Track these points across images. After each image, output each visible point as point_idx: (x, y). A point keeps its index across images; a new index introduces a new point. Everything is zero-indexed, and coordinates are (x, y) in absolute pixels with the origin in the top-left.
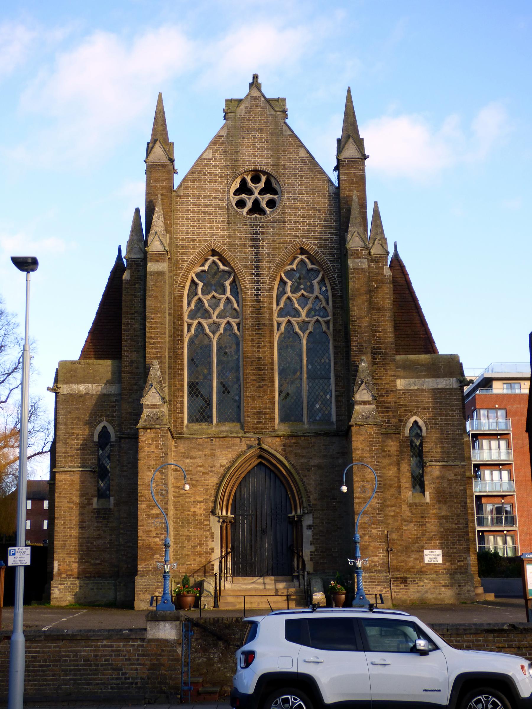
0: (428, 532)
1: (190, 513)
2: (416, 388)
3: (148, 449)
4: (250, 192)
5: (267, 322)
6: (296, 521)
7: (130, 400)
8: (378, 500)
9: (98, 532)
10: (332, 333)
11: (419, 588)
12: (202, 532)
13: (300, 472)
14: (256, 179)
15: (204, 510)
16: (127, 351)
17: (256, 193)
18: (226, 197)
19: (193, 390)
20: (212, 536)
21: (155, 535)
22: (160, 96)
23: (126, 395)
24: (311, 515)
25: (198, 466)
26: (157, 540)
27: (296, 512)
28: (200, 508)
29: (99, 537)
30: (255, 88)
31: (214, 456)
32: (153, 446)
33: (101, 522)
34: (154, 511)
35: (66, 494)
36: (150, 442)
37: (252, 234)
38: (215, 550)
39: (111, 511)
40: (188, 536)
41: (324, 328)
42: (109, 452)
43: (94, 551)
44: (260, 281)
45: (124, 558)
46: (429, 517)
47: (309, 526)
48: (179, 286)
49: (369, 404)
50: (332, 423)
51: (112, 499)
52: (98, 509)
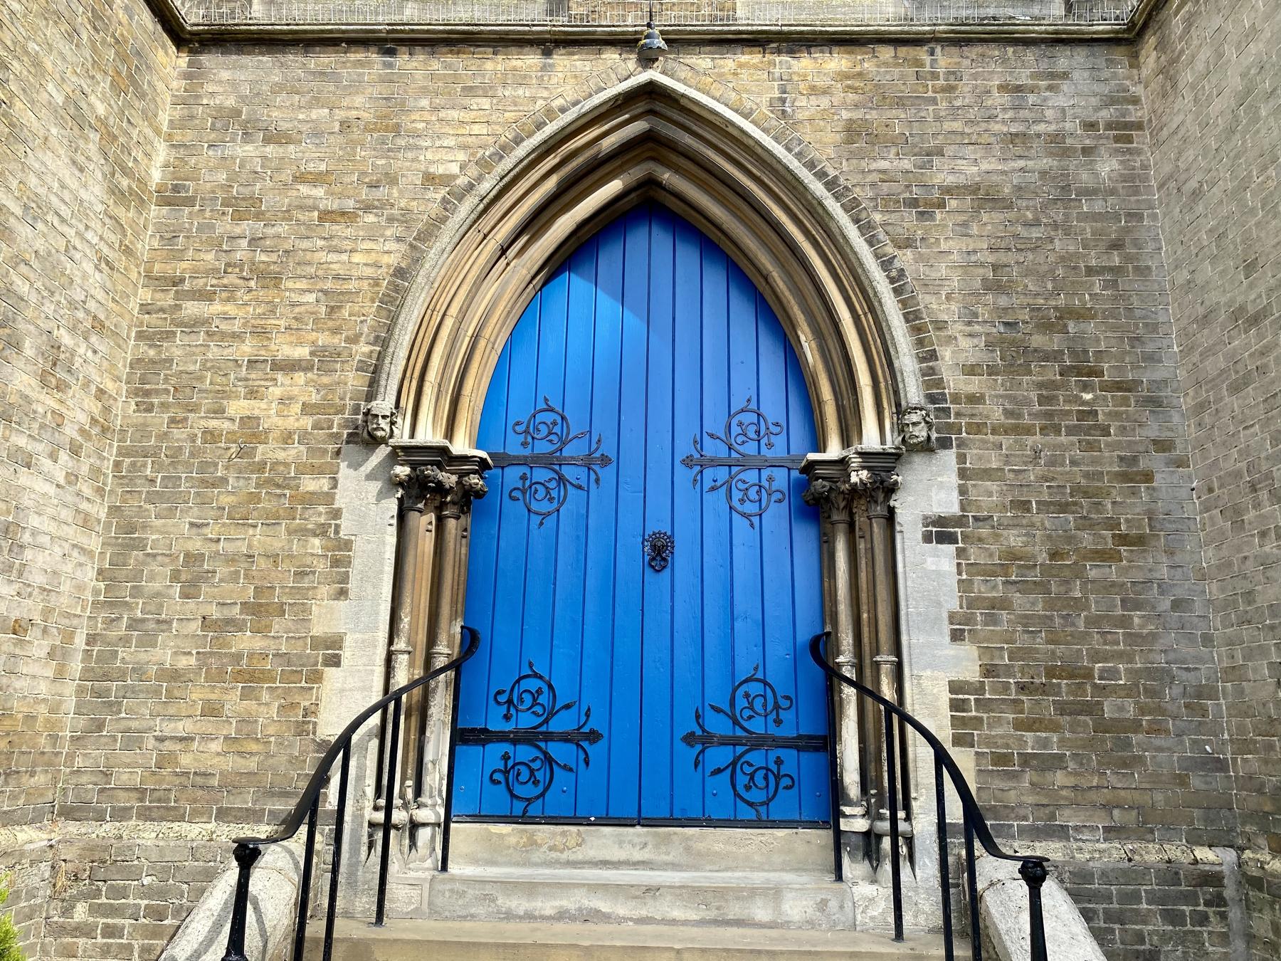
1: (227, 425)
6: (856, 492)
12: (278, 540)
13: (877, 217)
15: (307, 409)
20: (336, 563)
24: (948, 457)
25: (300, 178)
28: (284, 401)
31: (397, 129)
38: (346, 655)
40: (192, 558)
47: (940, 521)
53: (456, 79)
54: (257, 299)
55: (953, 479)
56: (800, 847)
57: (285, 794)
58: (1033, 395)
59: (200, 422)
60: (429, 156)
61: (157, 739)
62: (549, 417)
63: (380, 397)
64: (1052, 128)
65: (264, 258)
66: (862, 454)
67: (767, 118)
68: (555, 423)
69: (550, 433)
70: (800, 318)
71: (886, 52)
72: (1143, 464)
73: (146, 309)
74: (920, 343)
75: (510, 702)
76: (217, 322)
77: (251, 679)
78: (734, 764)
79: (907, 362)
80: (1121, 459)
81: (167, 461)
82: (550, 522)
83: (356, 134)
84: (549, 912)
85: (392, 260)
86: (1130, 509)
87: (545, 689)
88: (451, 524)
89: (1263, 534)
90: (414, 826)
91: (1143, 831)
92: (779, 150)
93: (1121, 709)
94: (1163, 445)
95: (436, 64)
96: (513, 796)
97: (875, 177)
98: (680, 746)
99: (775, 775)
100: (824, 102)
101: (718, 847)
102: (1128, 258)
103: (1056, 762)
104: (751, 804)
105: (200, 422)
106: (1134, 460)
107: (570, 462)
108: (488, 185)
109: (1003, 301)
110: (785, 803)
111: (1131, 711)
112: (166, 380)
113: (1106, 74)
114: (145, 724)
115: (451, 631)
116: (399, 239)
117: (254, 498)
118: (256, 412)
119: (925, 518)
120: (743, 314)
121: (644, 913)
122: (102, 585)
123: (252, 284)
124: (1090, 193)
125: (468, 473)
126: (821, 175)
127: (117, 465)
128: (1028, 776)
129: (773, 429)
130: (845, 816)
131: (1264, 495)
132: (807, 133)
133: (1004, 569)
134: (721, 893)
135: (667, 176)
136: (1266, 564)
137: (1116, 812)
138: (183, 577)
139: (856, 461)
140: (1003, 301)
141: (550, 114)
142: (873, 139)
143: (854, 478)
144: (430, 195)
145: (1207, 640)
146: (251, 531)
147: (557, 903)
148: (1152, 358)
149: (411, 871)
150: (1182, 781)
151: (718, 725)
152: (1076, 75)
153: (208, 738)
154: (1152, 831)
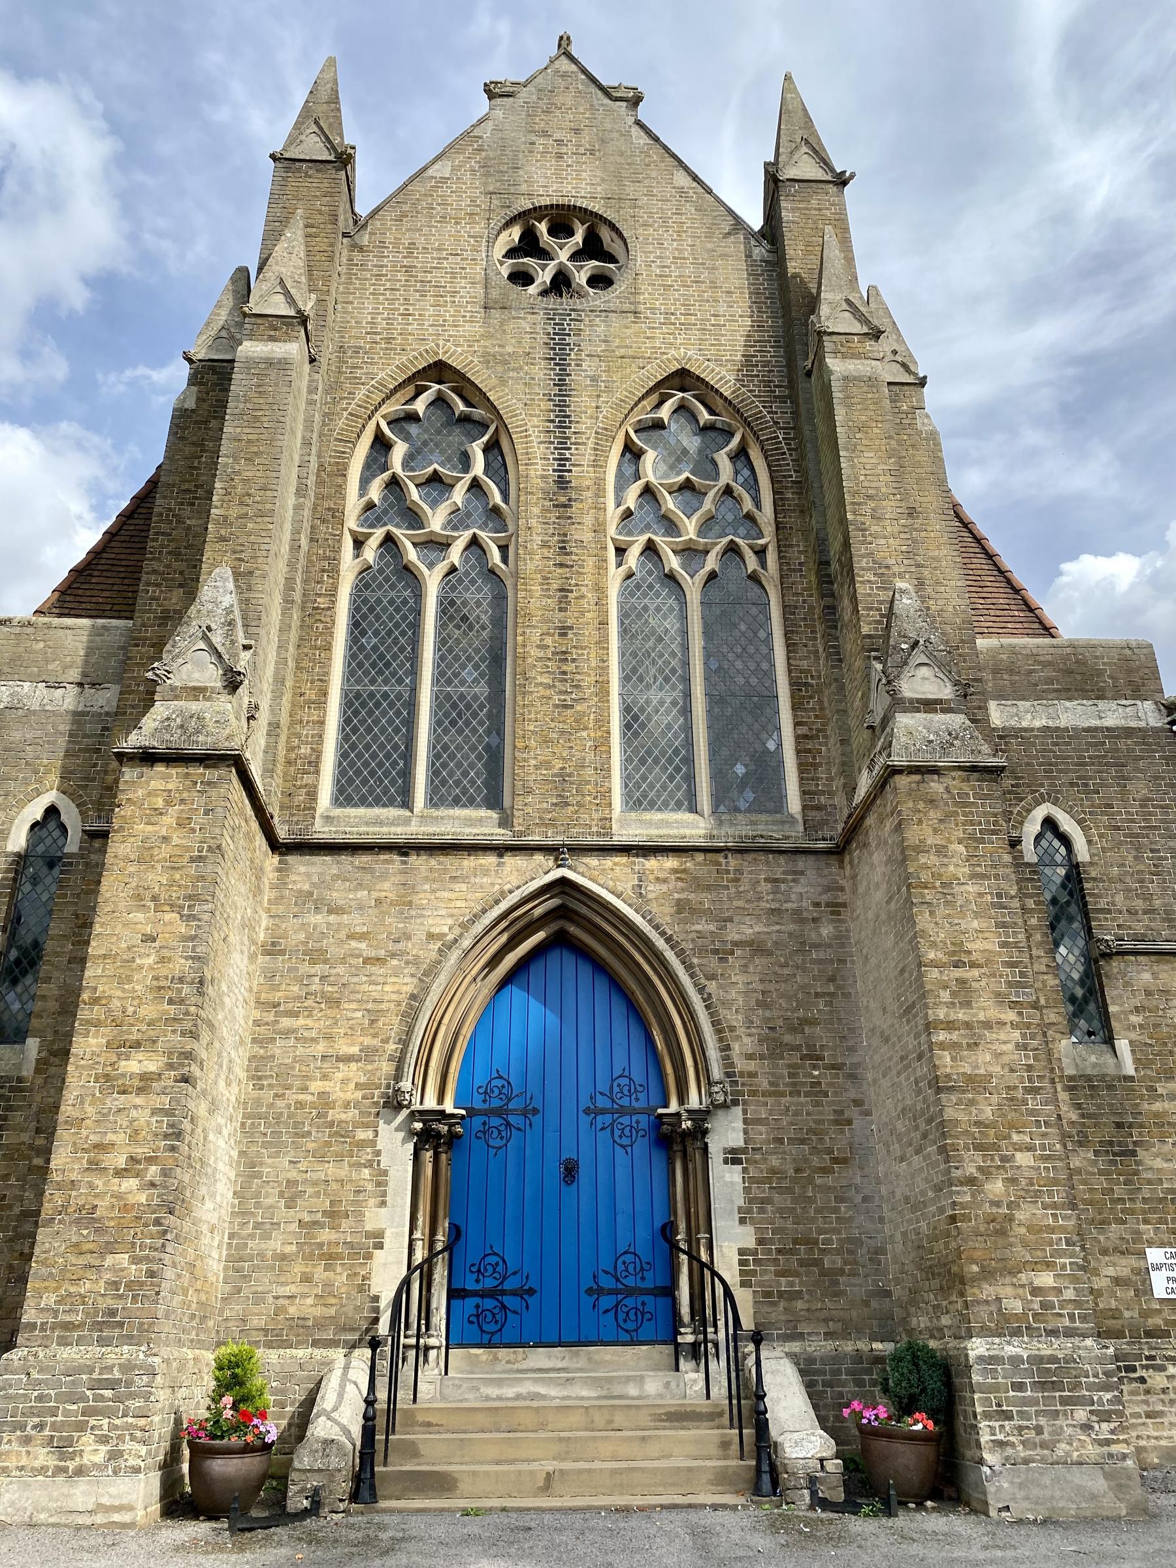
0: (1149, 1182)
1: (309, 1098)
2: (1037, 724)
4: (544, 254)
5: (587, 536)
6: (685, 1134)
8: (1023, 1035)
10: (777, 576)
11: (1152, 1399)
12: (343, 1171)
13: (695, 961)
14: (561, 229)
16: (158, 585)
17: (563, 256)
18: (484, 255)
19: (356, 713)
20: (379, 1184)
21: (121, 1161)
22: (788, 78)
23: (133, 707)
24: (738, 1111)
25: (350, 937)
26: (131, 1183)
27: (682, 1100)
31: (410, 903)
32: (169, 820)
34: (135, 1065)
36: (160, 803)
37: (549, 334)
38: (387, 1241)
39: (21, 1090)
40: (291, 1183)
41: (752, 563)
44: (569, 438)
46: (1141, 1126)
47: (733, 1151)
48: (336, 440)
49: (943, 711)
50: (792, 820)
54: (326, 1016)
55: (740, 1125)
56: (656, 1356)
57: (353, 1330)
58: (785, 1072)
59: (293, 1096)
60: (431, 922)
61: (274, 1297)
62: (499, 1083)
63: (404, 1079)
65: (330, 989)
66: (687, 1111)
67: (631, 897)
68: (503, 1087)
69: (500, 1093)
70: (653, 1020)
71: (700, 857)
72: (847, 1114)
73: (257, 1023)
74: (721, 1040)
75: (479, 1271)
76: (301, 1031)
77: (330, 1258)
78: (616, 1306)
79: (713, 1054)
80: (835, 1111)
81: (274, 1121)
82: (502, 1152)
83: (385, 907)
84: (510, 1395)
85: (409, 989)
86: (838, 1141)
87: (501, 1263)
88: (443, 1157)
90: (427, 1348)
91: (845, 1335)
92: (638, 919)
93: (834, 1262)
94: (858, 1103)
95: (433, 862)
96: (482, 1331)
97: (694, 935)
98: (582, 1116)
99: (641, 1312)
100: (664, 888)
101: (608, 1357)
102: (838, 987)
103: (797, 1295)
104: (627, 1331)
105: (293, 1096)
106: (842, 1112)
107: (513, 1112)
108: (467, 943)
109: (768, 1014)
110: (648, 1329)
111: (839, 1264)
112: (271, 1069)
113: (826, 872)
114: (267, 1289)
115: (444, 1225)
116: (412, 975)
117: (328, 1144)
118: (328, 1089)
119: (725, 1149)
120: (619, 1008)
121: (565, 1393)
122: (237, 1201)
123: (323, 1005)
125: (454, 1124)
126: (662, 934)
127: (243, 1124)
128: (782, 1304)
129: (639, 1088)
130: (681, 1334)
132: (654, 908)
133: (769, 1180)
134: (609, 1380)
135: (572, 929)
137: (831, 1323)
138: (286, 1195)
139: (684, 1116)
140: (768, 1014)
141: (503, 894)
142: (693, 911)
143: (684, 1126)
144: (431, 946)
145: (881, 1220)
146: (327, 1165)
147: (515, 1390)
148: (852, 1049)
149: (431, 1372)
150: (867, 1304)
151: (606, 1282)
152: (808, 873)
153: (304, 1296)
154: (850, 1334)
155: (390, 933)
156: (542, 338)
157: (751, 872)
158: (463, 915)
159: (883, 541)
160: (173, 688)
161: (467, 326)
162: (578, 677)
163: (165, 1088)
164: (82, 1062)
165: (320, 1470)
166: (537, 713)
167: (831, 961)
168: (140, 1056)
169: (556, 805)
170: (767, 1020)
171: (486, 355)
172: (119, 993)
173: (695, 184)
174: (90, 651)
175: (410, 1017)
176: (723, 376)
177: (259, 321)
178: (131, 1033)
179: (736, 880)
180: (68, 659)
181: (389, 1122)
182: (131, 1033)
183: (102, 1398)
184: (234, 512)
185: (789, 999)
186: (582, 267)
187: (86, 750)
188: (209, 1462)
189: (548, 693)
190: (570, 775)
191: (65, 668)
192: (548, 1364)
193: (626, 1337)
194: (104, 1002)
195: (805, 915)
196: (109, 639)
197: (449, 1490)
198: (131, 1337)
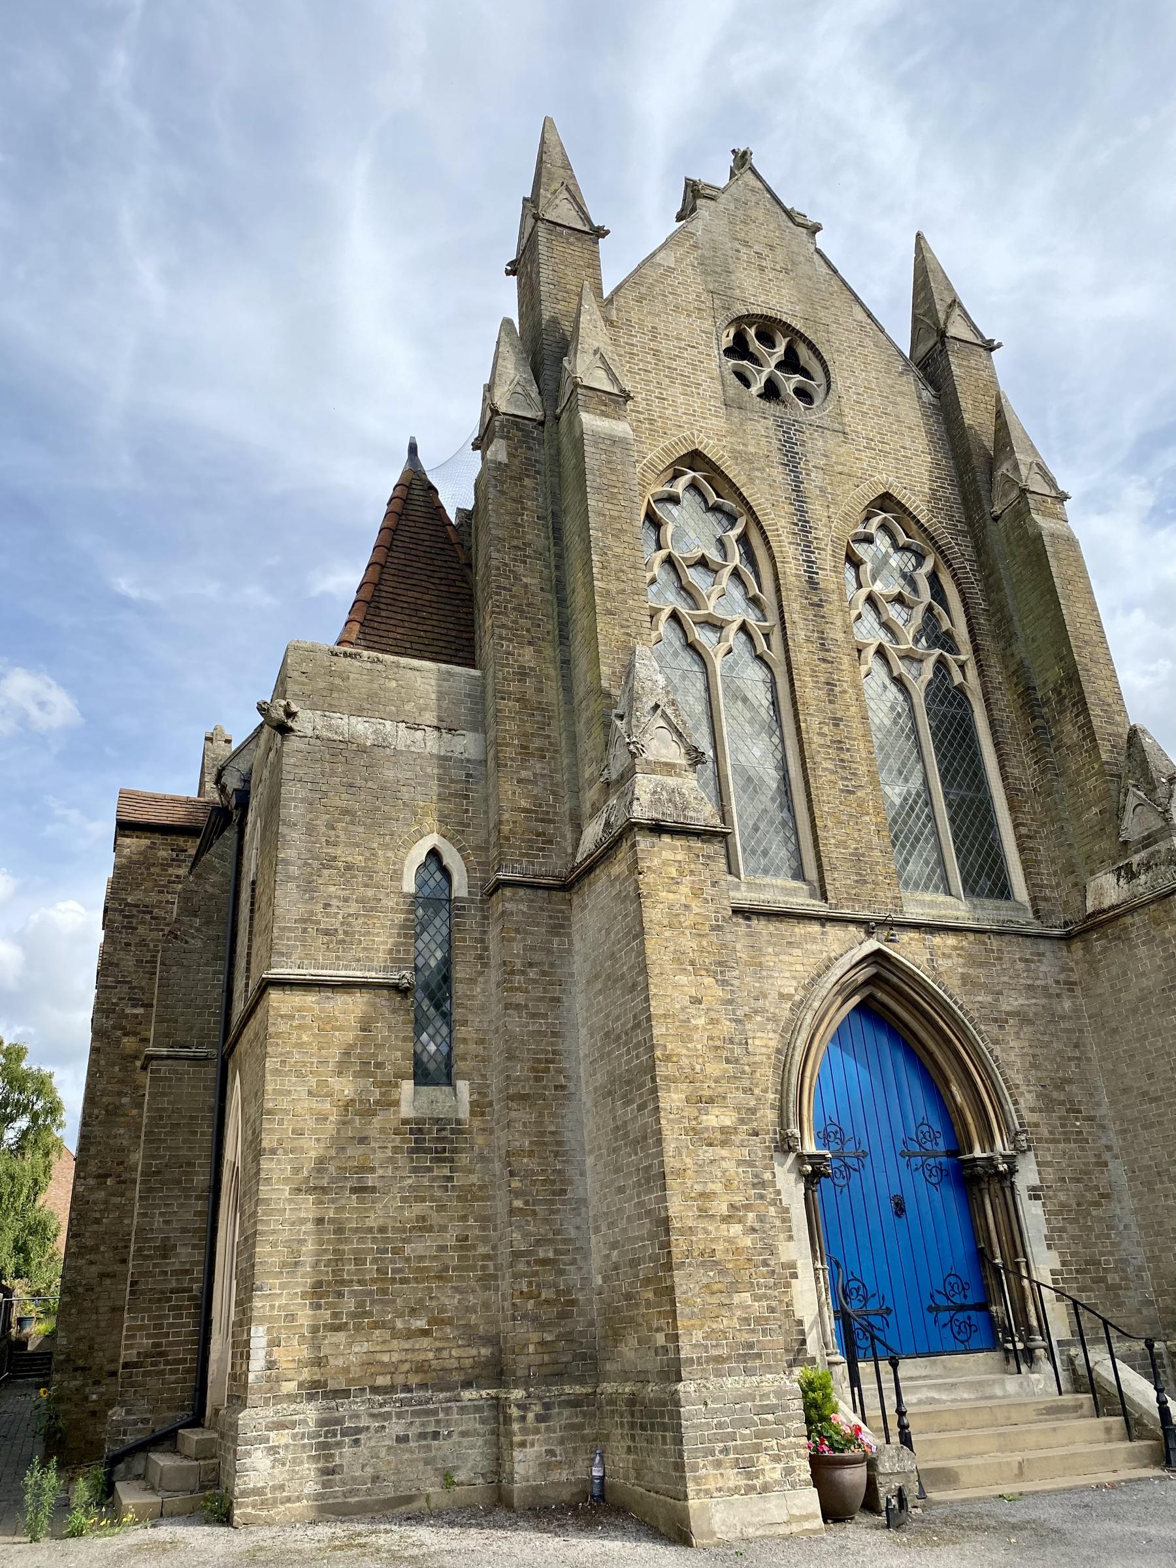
3: (671, 896)
7: (524, 774)
9: (419, 1208)
13: (983, 1027)
16: (511, 640)
20: (784, 1221)
21: (724, 1209)
23: (512, 759)
24: (1031, 1154)
26: (736, 1229)
29: (423, 1226)
30: (749, 172)
32: (684, 889)
33: (430, 1169)
34: (716, 1118)
35: (304, 1064)
36: (673, 872)
38: (799, 1271)
39: (461, 1132)
42: (445, 931)
43: (403, 1281)
45: (531, 1304)
47: (1034, 1189)
50: (1020, 907)
51: (463, 1086)
52: (418, 1121)
53: (783, 937)
55: (1034, 1167)
64: (1043, 983)
71: (971, 937)
84: (915, 1401)
89: (1166, 1196)
97: (977, 1005)
100: (950, 962)
101: (957, 1365)
102: (1082, 1053)
116: (774, 1031)
124: (1062, 1018)
131: (1165, 1179)
135: (880, 995)
136: (1168, 1209)
142: (974, 984)
144: (784, 1005)
150: (1139, 1311)
151: (941, 1301)
155: (749, 991)
156: (776, 444)
157: (1009, 952)
158: (804, 978)
159: (1102, 683)
160: (647, 762)
161: (714, 420)
162: (855, 766)
163: (742, 1141)
164: (671, 1116)
165: (898, 1473)
166: (829, 796)
167: (1073, 1031)
168: (716, 1111)
169: (856, 881)
170: (1039, 1079)
171: (733, 451)
172: (684, 1051)
173: (869, 321)
174: (441, 695)
175: (784, 1069)
176: (917, 504)
177: (590, 393)
178: (703, 1090)
179: (1000, 959)
180: (422, 701)
181: (782, 1165)
182: (703, 1090)
183: (767, 1422)
184: (614, 587)
185: (1053, 1060)
186: (789, 379)
187: (456, 795)
188: (839, 1472)
189: (833, 778)
190: (863, 855)
191: (421, 710)
192: (916, 1373)
193: (961, 1347)
194: (675, 1059)
195: (1051, 991)
196: (455, 685)
197: (954, 1482)
198: (770, 1366)
